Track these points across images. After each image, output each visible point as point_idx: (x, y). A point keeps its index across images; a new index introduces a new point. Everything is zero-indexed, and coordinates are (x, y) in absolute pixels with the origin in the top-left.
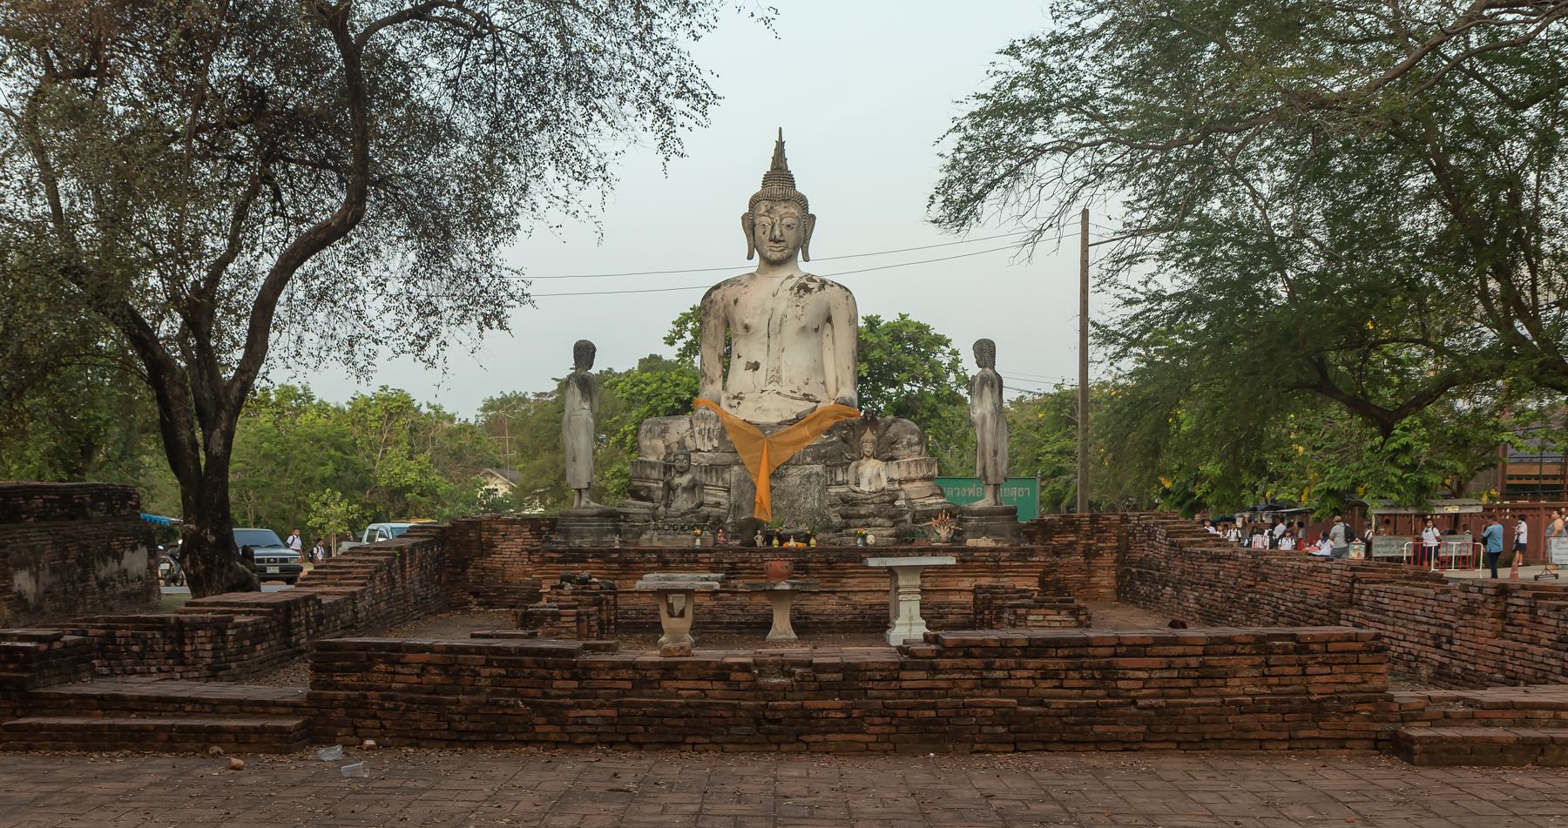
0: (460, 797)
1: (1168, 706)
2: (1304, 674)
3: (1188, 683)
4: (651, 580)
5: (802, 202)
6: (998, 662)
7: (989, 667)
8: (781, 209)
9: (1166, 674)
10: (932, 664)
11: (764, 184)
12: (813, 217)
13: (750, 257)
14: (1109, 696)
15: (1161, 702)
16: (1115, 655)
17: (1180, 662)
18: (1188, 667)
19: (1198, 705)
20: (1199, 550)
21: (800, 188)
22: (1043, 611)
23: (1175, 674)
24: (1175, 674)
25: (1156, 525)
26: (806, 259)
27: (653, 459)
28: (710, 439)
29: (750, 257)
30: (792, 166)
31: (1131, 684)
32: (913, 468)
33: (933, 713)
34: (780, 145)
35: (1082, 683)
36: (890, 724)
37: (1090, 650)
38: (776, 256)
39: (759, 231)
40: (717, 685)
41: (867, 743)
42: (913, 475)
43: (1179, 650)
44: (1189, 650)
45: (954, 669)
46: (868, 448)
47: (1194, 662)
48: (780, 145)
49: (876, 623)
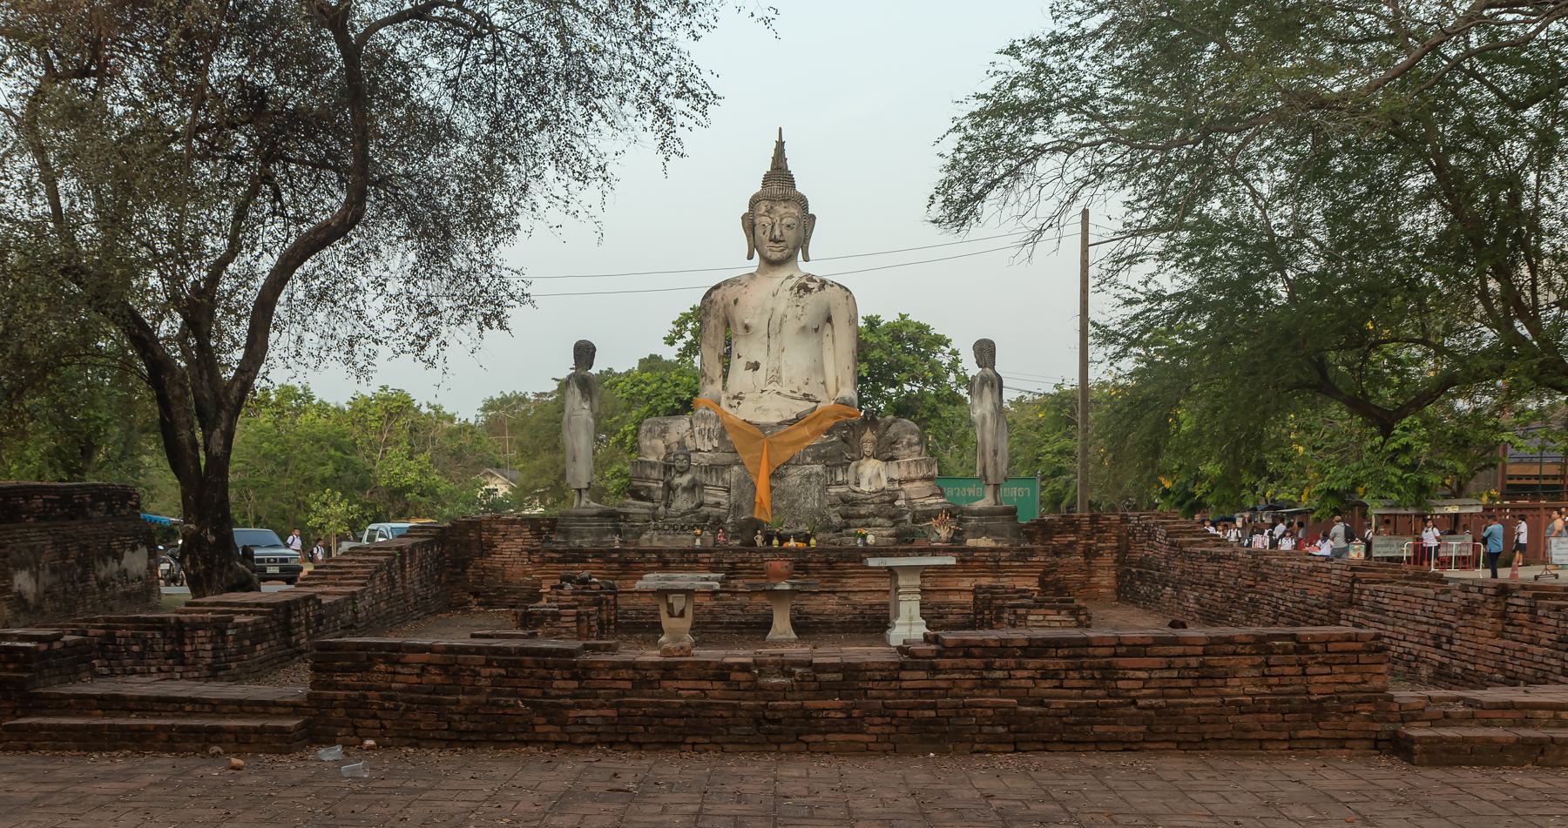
1: (1168, 706)
2: (1304, 674)
3: (1188, 683)
4: (651, 580)
5: (802, 202)
6: (998, 662)
7: (989, 667)
8: (781, 209)
9: (1166, 674)
10: (932, 664)
11: (764, 184)
12: (813, 217)
13: (750, 257)
14: (1109, 696)
15: (1161, 702)
16: (1115, 655)
17: (1180, 662)
18: (1188, 667)
19: (1198, 705)
20: (1199, 550)
21: (800, 188)
22: (1043, 611)
23: (1175, 674)
24: (1175, 674)
25: (1156, 525)
26: (806, 259)
27: (653, 459)
28: (710, 439)
29: (750, 257)
30: (792, 166)
31: (1131, 684)
32: (913, 468)
33: (933, 713)
34: (780, 145)
35: (1082, 683)
36: (890, 724)
37: (1090, 650)
38: (776, 256)
39: (759, 231)
40: (717, 685)
41: (867, 743)
42: (913, 475)
43: (1179, 650)
44: (1189, 650)
45: (954, 669)
46: (868, 448)
47: (1194, 662)
48: (780, 145)
49: (876, 623)
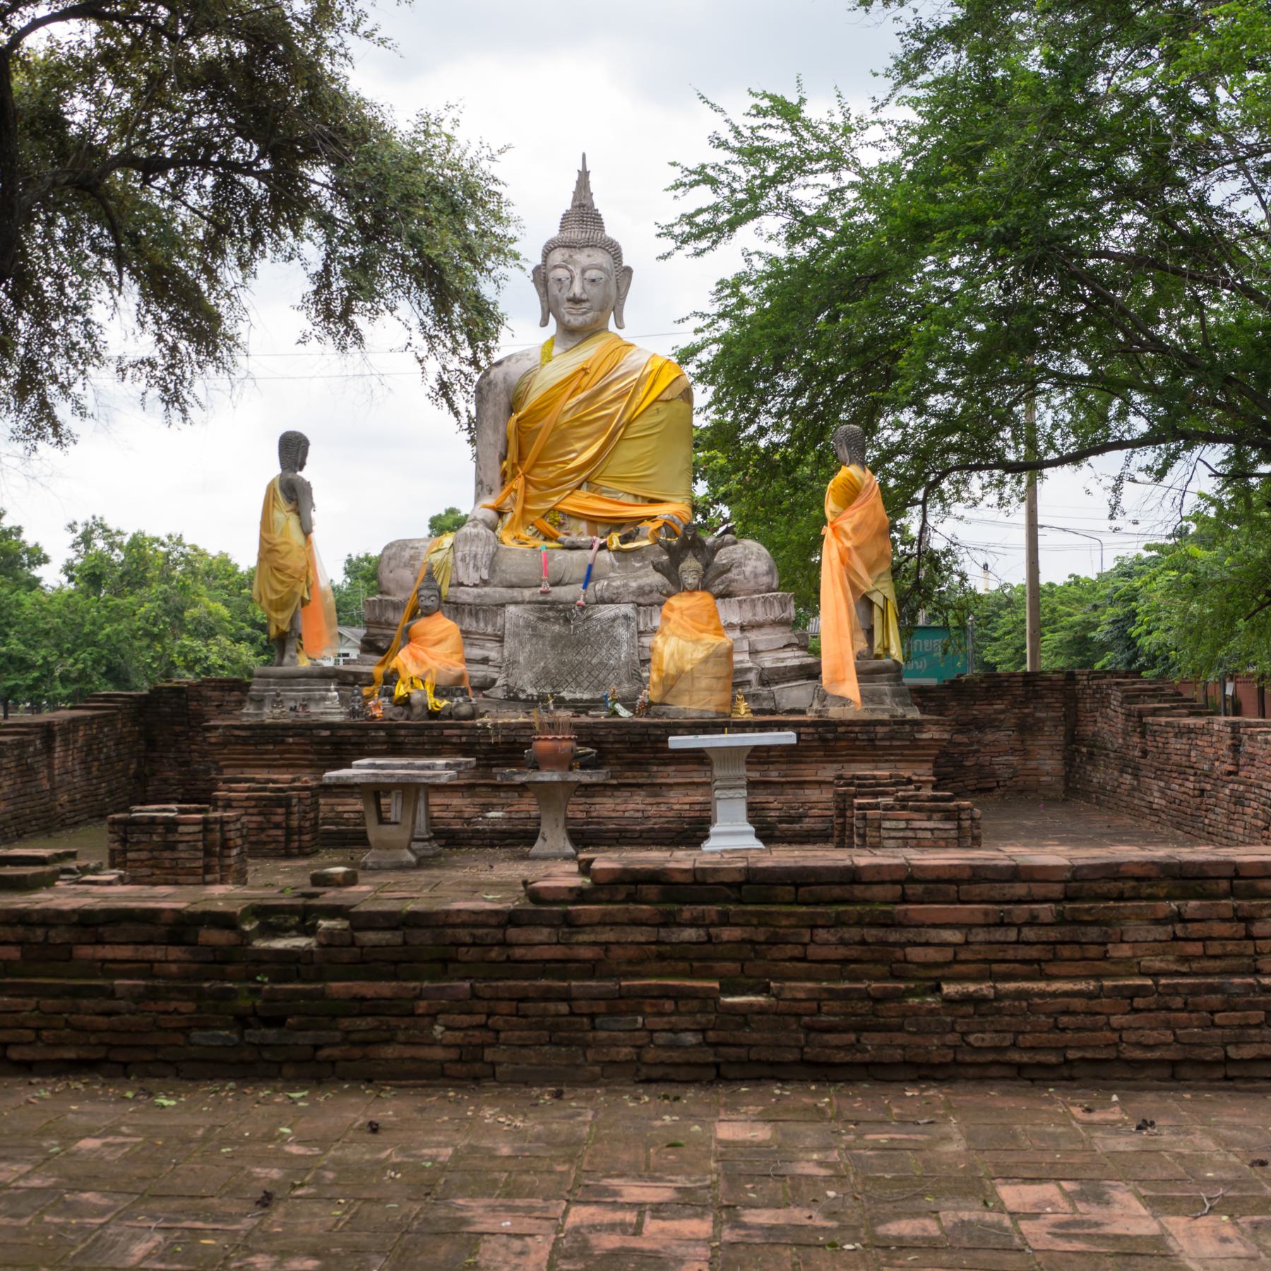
0: (948, 954)
1: (999, 997)
2: (1250, 937)
3: (1034, 952)
4: (359, 770)
5: (613, 250)
6: (688, 912)
7: (669, 921)
8: (583, 258)
9: (999, 935)
10: (566, 915)
11: (563, 227)
12: (628, 271)
13: (544, 323)
14: (895, 977)
15: (986, 988)
16: (904, 899)
17: (1021, 912)
18: (1033, 922)
19: (1054, 995)
20: (1163, 720)
21: (611, 231)
22: (905, 814)
23: (1012, 935)
24: (1012, 935)
25: (1109, 686)
26: (620, 325)
27: (398, 597)
28: (476, 568)
29: (544, 323)
30: (599, 203)
31: (931, 954)
32: (760, 609)
33: (563, 1008)
34: (584, 176)
35: (842, 952)
36: (484, 1026)
37: (858, 891)
38: (576, 321)
39: (554, 289)
40: (175, 952)
41: (442, 1063)
42: (760, 617)
43: (1020, 889)
44: (1039, 890)
45: (606, 922)
46: (690, 579)
47: (1045, 911)
48: (584, 176)
49: (694, 831)
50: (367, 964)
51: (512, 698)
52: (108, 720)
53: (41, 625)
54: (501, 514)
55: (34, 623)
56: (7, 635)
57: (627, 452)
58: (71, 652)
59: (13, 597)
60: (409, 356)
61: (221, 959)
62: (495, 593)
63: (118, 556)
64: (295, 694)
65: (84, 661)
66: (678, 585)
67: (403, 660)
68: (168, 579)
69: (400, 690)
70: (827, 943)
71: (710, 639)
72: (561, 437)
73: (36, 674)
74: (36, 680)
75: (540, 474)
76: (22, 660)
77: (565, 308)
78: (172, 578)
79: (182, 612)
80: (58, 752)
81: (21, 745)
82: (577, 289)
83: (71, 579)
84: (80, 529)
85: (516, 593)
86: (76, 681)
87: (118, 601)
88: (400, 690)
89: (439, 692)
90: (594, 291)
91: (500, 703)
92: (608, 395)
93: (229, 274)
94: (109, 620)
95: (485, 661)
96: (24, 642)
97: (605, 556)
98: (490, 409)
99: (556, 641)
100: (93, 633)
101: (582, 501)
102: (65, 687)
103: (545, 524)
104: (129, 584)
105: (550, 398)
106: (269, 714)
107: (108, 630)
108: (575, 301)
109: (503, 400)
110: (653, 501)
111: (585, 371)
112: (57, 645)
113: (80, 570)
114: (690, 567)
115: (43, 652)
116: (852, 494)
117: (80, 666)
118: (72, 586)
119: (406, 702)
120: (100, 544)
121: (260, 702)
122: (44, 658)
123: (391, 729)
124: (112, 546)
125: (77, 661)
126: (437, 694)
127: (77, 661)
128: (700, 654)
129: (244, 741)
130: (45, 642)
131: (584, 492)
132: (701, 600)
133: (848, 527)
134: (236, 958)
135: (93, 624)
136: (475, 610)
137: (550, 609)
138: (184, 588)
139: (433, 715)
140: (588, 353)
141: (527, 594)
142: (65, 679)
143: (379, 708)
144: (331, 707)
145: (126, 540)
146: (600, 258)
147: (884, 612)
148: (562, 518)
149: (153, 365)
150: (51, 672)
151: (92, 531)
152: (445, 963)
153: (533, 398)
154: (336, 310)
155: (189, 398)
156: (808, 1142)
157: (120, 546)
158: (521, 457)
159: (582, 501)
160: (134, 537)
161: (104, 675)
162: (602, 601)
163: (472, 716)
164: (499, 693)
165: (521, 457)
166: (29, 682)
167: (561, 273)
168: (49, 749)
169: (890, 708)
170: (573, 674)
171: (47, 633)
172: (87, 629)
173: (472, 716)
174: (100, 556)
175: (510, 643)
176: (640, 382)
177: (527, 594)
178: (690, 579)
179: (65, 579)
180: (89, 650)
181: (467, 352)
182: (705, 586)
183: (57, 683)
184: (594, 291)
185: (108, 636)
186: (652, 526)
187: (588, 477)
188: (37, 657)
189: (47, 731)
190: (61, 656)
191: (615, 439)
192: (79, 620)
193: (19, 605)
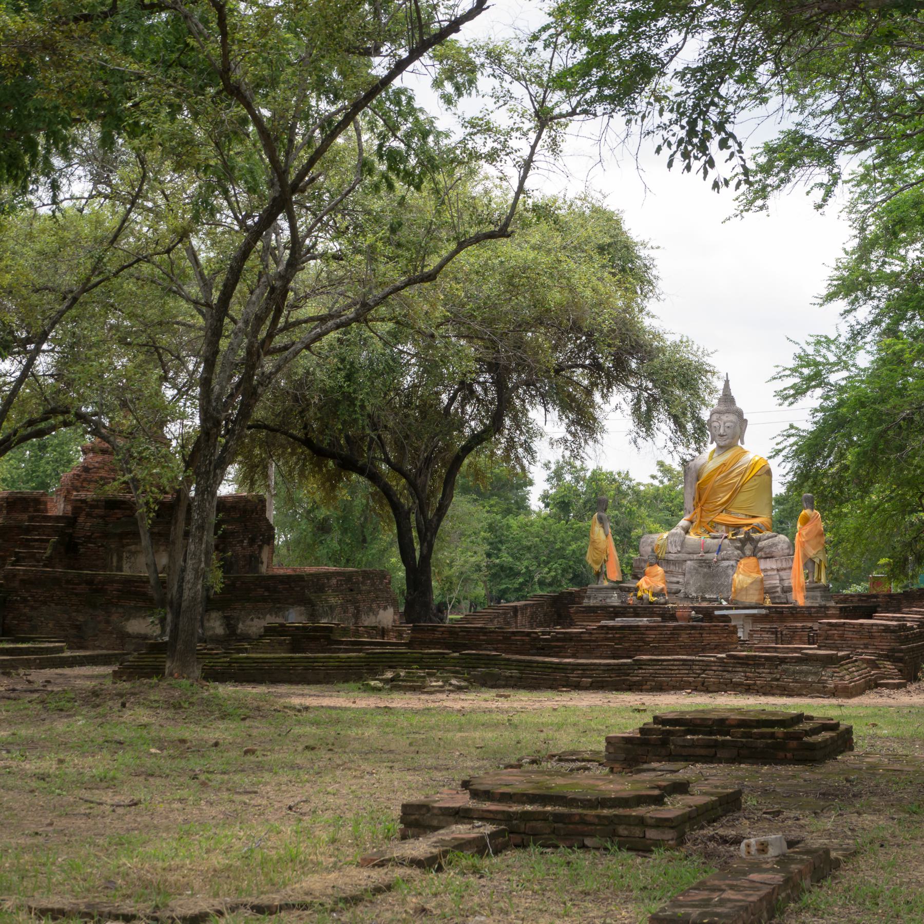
5: (739, 414)
8: (724, 418)
26: (743, 443)
46: (748, 552)
50: (558, 640)
51: (686, 597)
52: (540, 605)
53: (525, 543)
54: (692, 522)
55: (519, 541)
56: (500, 550)
57: (741, 497)
58: (546, 563)
59: (504, 521)
60: (666, 451)
61: (535, 639)
62: (682, 556)
63: (582, 487)
64: (601, 595)
65: (556, 569)
66: (744, 556)
67: (642, 583)
68: (618, 506)
69: (639, 594)
70: (633, 637)
71: (755, 575)
72: (714, 492)
73: (521, 580)
74: (521, 584)
75: (707, 507)
76: (511, 569)
77: (717, 438)
78: (621, 506)
79: (630, 532)
80: (519, 617)
81: (505, 614)
82: (722, 431)
83: (547, 505)
84: (553, 467)
85: (691, 556)
86: (550, 585)
87: (581, 524)
88: (639, 594)
89: (653, 595)
90: (728, 431)
91: (681, 599)
92: (733, 474)
93: (597, 397)
94: (575, 539)
95: (678, 583)
96: (512, 556)
97: (726, 541)
98: (689, 479)
99: (705, 575)
100: (563, 548)
101: (724, 518)
102: (542, 590)
103: (709, 527)
104: (590, 510)
105: (710, 476)
106: (592, 603)
107: (574, 546)
108: (721, 436)
109: (694, 475)
110: (754, 517)
111: (724, 464)
112: (536, 558)
113: (553, 499)
114: (748, 548)
115: (526, 563)
116: (806, 520)
117: (553, 574)
118: (548, 511)
119: (641, 598)
120: (568, 477)
121: (589, 598)
122: (527, 568)
123: (635, 608)
124: (577, 480)
125: (550, 570)
126: (653, 595)
127: (550, 570)
128: (749, 581)
129: (583, 612)
130: (528, 555)
131: (724, 514)
132: (753, 560)
133: (804, 533)
134: (537, 639)
135: (562, 542)
136: (675, 562)
137: (704, 563)
138: (631, 513)
139: (651, 603)
140: (728, 455)
141: (695, 556)
142: (541, 583)
143: (631, 599)
144: (614, 600)
145: (589, 474)
146: (732, 418)
147: (819, 566)
148: (715, 525)
149: (566, 441)
150: (532, 578)
151: (562, 468)
152: (571, 640)
153: (704, 475)
154: (644, 420)
155: (583, 455)
156: (232, 443)
157: (584, 479)
158: (700, 499)
159: (724, 518)
160: (594, 472)
161: (571, 580)
162: (724, 559)
163: (666, 603)
164: (681, 595)
165: (700, 499)
166: (516, 586)
167: (715, 424)
168: (516, 615)
169: (819, 602)
170: (711, 588)
171: (529, 549)
172: (558, 546)
173: (666, 603)
174: (570, 488)
175: (687, 576)
176: (747, 469)
177: (695, 556)
178: (748, 552)
179: (542, 505)
180: (560, 561)
181: (693, 446)
182: (754, 554)
183: (537, 587)
184: (728, 431)
185: (574, 551)
186: (746, 529)
187: (726, 507)
188: (522, 567)
189: (515, 609)
190: (539, 566)
191: (736, 492)
192: (552, 539)
193: (509, 527)
